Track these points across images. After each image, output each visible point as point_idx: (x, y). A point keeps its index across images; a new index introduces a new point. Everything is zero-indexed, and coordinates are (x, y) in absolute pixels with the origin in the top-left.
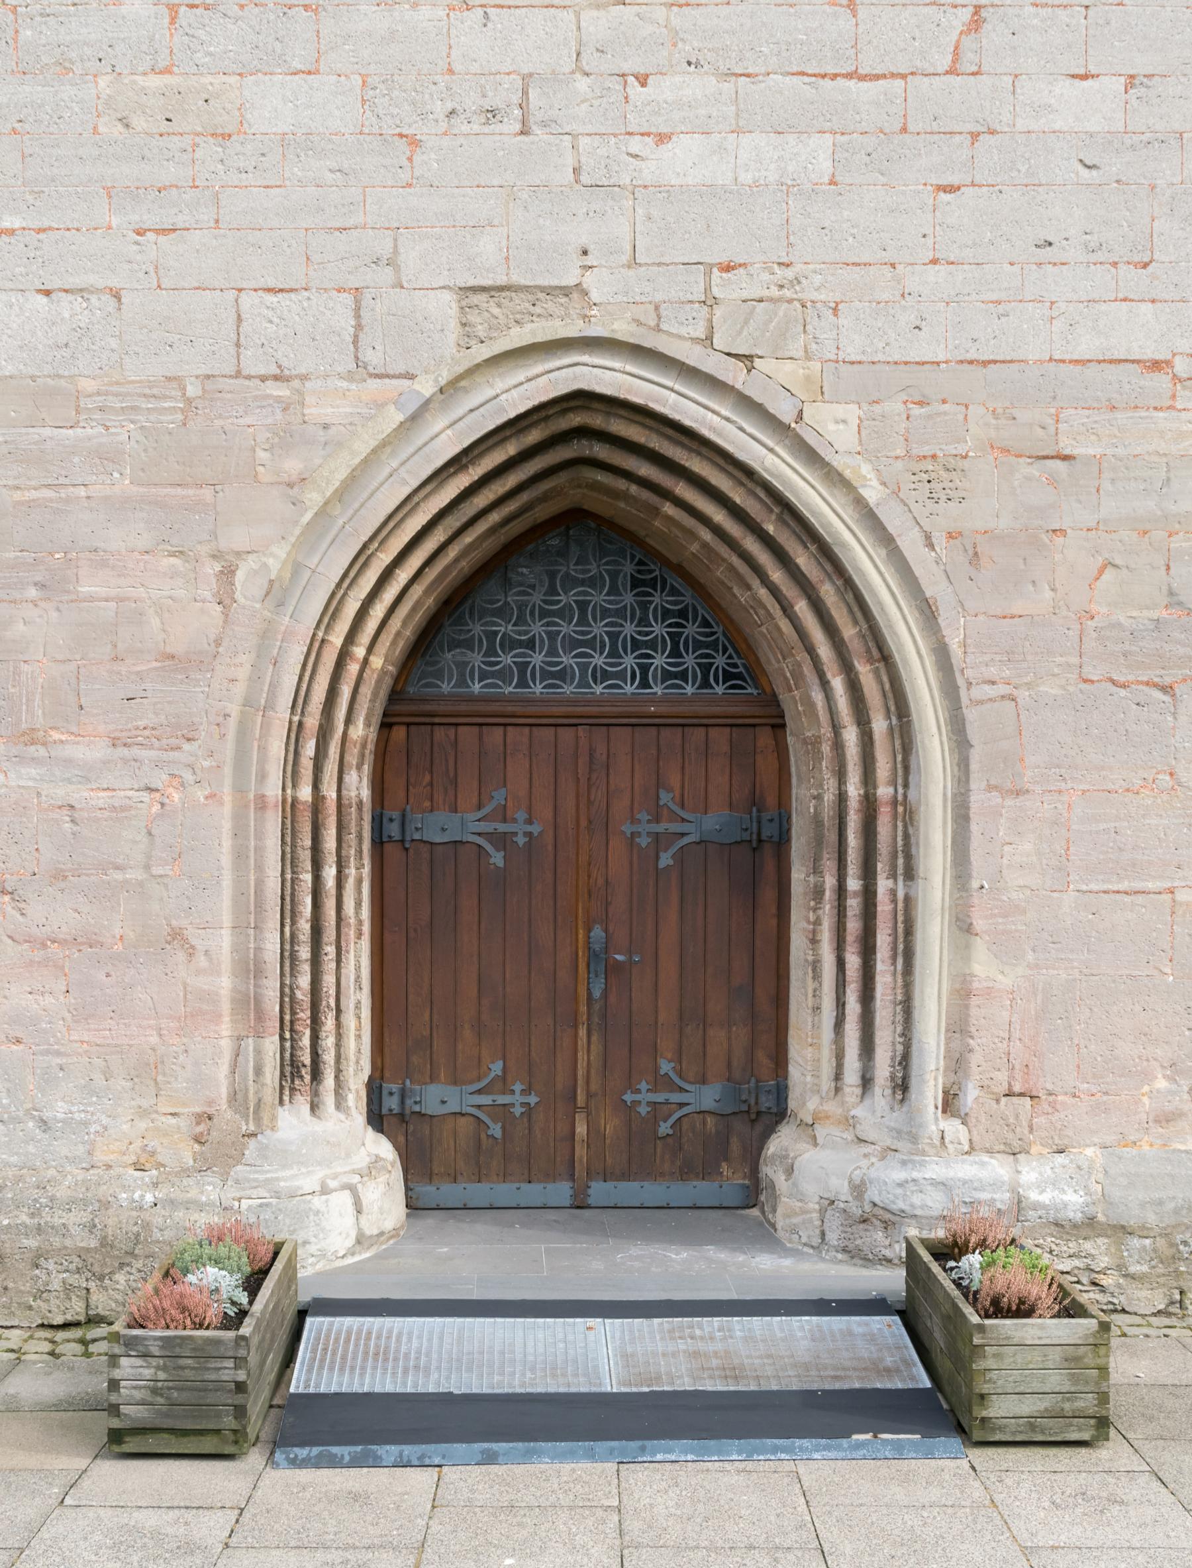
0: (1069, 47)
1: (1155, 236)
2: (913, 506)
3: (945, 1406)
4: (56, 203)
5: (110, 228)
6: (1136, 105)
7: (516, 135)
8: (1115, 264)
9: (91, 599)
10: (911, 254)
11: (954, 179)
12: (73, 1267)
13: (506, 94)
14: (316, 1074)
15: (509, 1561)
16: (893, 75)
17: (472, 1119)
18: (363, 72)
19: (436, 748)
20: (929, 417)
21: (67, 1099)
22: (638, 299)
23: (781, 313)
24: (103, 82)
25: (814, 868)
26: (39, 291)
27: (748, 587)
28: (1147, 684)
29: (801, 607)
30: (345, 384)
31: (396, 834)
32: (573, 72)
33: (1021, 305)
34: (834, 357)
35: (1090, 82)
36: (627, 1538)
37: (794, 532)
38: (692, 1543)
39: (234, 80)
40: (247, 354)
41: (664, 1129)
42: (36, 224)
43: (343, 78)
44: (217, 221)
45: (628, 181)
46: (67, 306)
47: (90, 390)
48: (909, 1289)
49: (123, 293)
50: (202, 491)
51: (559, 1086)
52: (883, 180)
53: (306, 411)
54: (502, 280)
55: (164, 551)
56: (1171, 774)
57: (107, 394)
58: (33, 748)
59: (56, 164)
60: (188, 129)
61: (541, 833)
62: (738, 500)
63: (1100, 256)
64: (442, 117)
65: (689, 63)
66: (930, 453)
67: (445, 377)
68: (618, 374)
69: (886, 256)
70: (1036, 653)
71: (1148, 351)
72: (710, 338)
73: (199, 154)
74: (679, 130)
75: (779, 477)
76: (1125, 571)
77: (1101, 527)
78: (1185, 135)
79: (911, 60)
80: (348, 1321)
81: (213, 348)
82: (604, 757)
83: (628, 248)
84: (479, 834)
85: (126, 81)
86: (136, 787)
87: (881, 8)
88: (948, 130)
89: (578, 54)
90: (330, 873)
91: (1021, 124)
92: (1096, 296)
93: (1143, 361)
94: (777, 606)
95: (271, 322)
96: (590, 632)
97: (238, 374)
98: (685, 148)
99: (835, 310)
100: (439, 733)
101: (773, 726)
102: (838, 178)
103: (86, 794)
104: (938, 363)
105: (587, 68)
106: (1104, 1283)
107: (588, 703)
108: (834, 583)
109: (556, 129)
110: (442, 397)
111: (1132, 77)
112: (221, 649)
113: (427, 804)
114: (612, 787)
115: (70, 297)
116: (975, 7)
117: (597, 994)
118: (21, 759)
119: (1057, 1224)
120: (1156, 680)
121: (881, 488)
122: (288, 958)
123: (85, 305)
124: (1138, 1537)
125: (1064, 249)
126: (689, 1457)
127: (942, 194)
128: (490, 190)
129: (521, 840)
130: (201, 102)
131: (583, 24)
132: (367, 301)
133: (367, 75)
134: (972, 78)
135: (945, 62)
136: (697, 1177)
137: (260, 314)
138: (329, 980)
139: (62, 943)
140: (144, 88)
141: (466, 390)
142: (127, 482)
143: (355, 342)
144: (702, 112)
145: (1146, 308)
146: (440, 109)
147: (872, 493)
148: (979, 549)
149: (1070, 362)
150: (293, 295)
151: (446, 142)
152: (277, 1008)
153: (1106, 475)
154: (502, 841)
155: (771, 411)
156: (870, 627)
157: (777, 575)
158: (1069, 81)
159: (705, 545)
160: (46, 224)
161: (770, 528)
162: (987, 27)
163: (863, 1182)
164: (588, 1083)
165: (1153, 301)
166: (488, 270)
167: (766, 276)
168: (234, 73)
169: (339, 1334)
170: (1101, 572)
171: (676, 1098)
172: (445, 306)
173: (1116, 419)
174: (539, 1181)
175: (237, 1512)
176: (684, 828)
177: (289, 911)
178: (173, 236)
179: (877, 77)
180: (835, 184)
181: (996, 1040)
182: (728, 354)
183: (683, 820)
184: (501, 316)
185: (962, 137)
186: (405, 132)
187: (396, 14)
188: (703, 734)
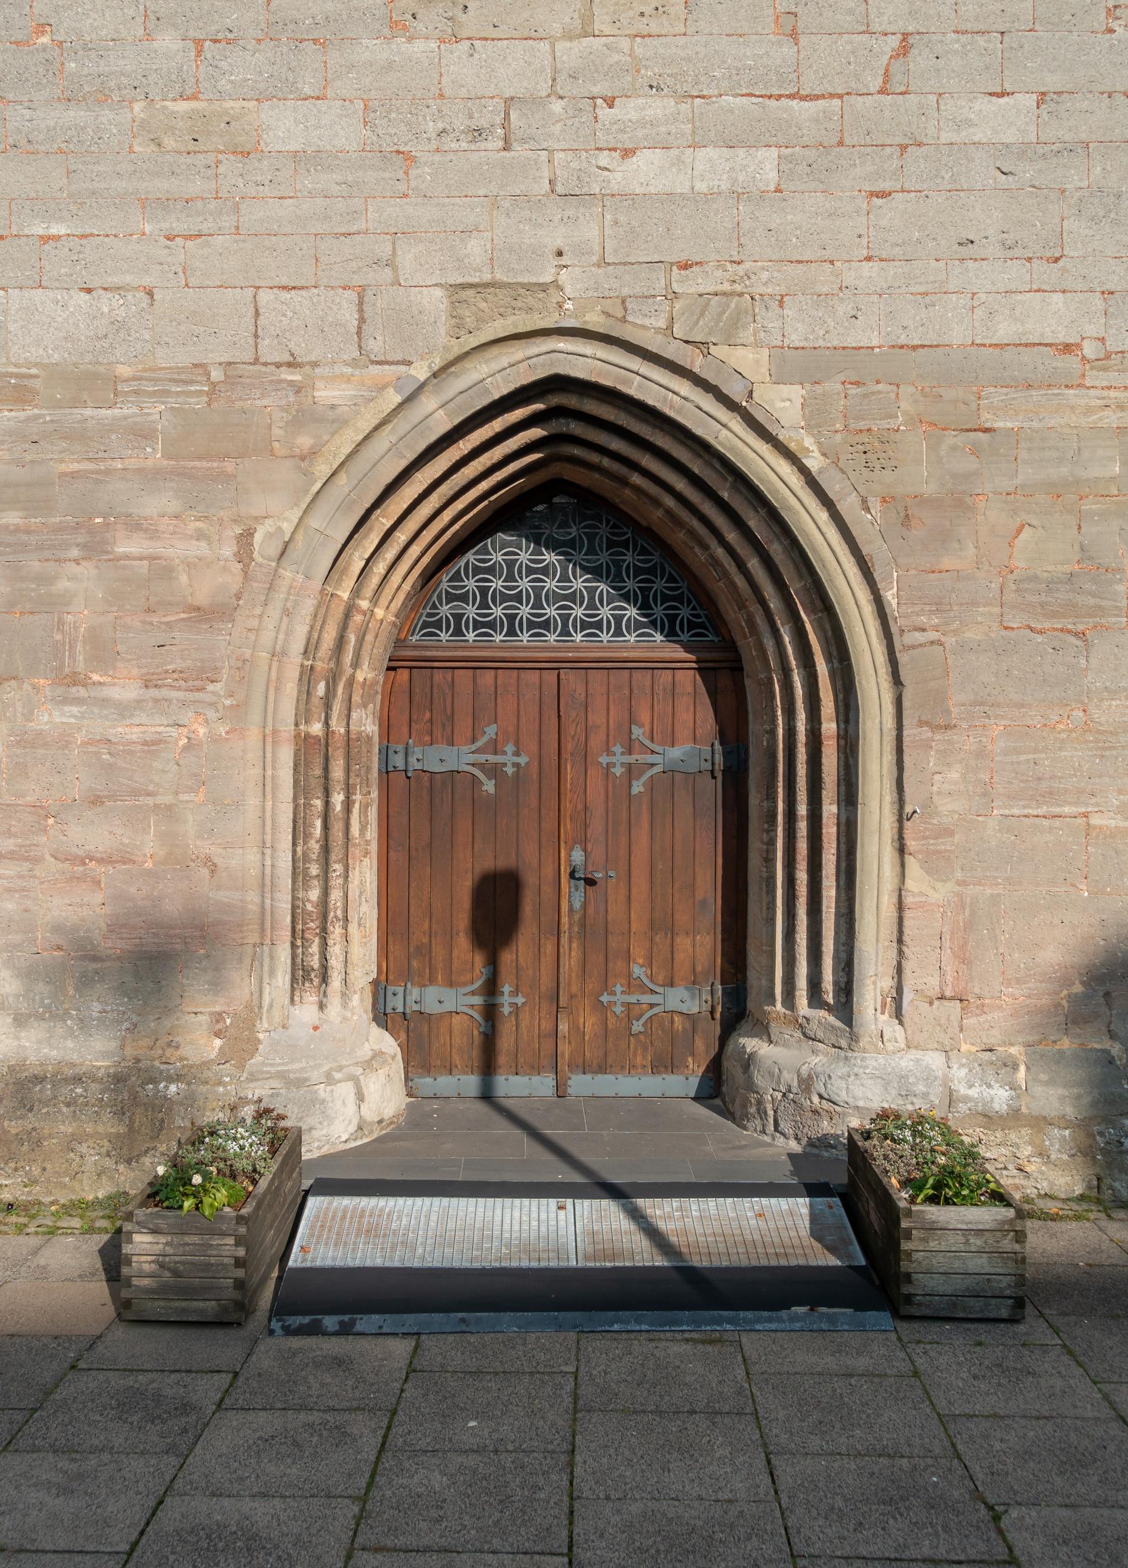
0: (987, 68)
1: (1065, 234)
2: (851, 474)
3: (877, 1283)
4: (97, 212)
5: (144, 234)
6: (1046, 118)
7: (499, 151)
8: (1029, 259)
9: (127, 557)
10: (848, 252)
11: (886, 186)
12: (104, 1150)
13: (489, 115)
14: (325, 979)
15: (472, 1424)
16: (832, 96)
17: (466, 1017)
18: (365, 97)
19: (435, 690)
20: (865, 396)
21: (102, 999)
22: (606, 294)
23: (733, 305)
24: (137, 107)
25: (767, 795)
26: (81, 289)
27: (705, 547)
28: (1062, 630)
29: (754, 564)
30: (350, 370)
31: (400, 765)
32: (549, 96)
33: (946, 296)
34: (780, 344)
35: (1005, 99)
36: (581, 1402)
37: (746, 498)
38: (638, 1407)
39: (252, 104)
40: (264, 343)
41: (637, 1027)
42: (79, 231)
43: (347, 103)
44: (237, 228)
45: (597, 191)
46: (106, 303)
47: (126, 375)
48: (850, 1176)
49: (155, 291)
50: (225, 464)
51: (543, 989)
52: (822, 187)
53: (316, 394)
54: (487, 277)
55: (191, 516)
56: (1084, 711)
57: (140, 379)
58: (74, 689)
59: (97, 179)
60: (211, 148)
61: (527, 764)
62: (696, 471)
63: (1017, 252)
64: (434, 135)
65: (651, 87)
66: (866, 427)
67: (438, 363)
68: (589, 360)
69: (828, 254)
70: (962, 604)
71: (1060, 335)
72: (670, 327)
73: (221, 169)
74: (642, 145)
75: (732, 449)
76: (1041, 530)
77: (1019, 492)
78: (1091, 145)
79: (846, 82)
80: (346, 1202)
81: (234, 339)
82: (583, 695)
83: (597, 248)
84: (473, 765)
85: (158, 106)
86: (165, 723)
87: (819, 37)
88: (880, 143)
89: (554, 80)
90: (338, 799)
91: (945, 137)
92: (1013, 287)
93: (1056, 345)
94: (733, 563)
95: (284, 315)
96: (571, 587)
97: (256, 361)
98: (646, 162)
99: (781, 304)
100: (438, 676)
101: (732, 669)
102: (782, 187)
103: (120, 730)
104: (872, 348)
105: (561, 93)
106: (1028, 1169)
107: (569, 650)
108: (781, 543)
109: (532, 145)
110: (435, 381)
111: (1043, 94)
112: (241, 602)
113: (427, 738)
114: (590, 723)
115: (109, 295)
116: (903, 34)
117: (577, 905)
118: (66, 701)
119: (985, 1116)
120: (1069, 627)
121: (822, 458)
122: (298, 874)
123: (121, 302)
124: (1046, 1407)
125: (984, 246)
126: (644, 1327)
127: (875, 199)
128: (477, 199)
129: (510, 770)
130: (223, 125)
131: (558, 54)
132: (369, 297)
133: (368, 100)
134: (901, 97)
135: (876, 84)
136: (666, 1071)
137: (275, 309)
138: (336, 895)
139: (100, 861)
140: (173, 112)
141: (456, 375)
142: (159, 456)
143: (359, 333)
144: (663, 129)
145: (1057, 298)
146: (432, 128)
147: (814, 462)
148: (910, 512)
149: (990, 346)
150: (303, 293)
151: (437, 157)
152: (289, 919)
153: (1023, 445)
154: (493, 771)
155: (725, 391)
156: (814, 581)
157: (732, 536)
158: (988, 98)
159: (669, 512)
160: (88, 231)
161: (725, 495)
162: (914, 51)
163: (810, 1077)
164: (570, 985)
165: (1064, 292)
166: (475, 270)
167: (719, 273)
168: (252, 99)
169: (335, 1212)
170: (1019, 531)
171: (647, 999)
172: (435, 300)
173: (1031, 396)
174: (526, 1074)
175: (231, 1376)
176: (651, 758)
177: (299, 831)
178: (199, 241)
179: (817, 97)
180: (780, 191)
181: (929, 949)
182: (687, 342)
183: (653, 752)
184: (487, 310)
185: (892, 149)
186: (401, 149)
187: (394, 46)
188: (670, 677)
